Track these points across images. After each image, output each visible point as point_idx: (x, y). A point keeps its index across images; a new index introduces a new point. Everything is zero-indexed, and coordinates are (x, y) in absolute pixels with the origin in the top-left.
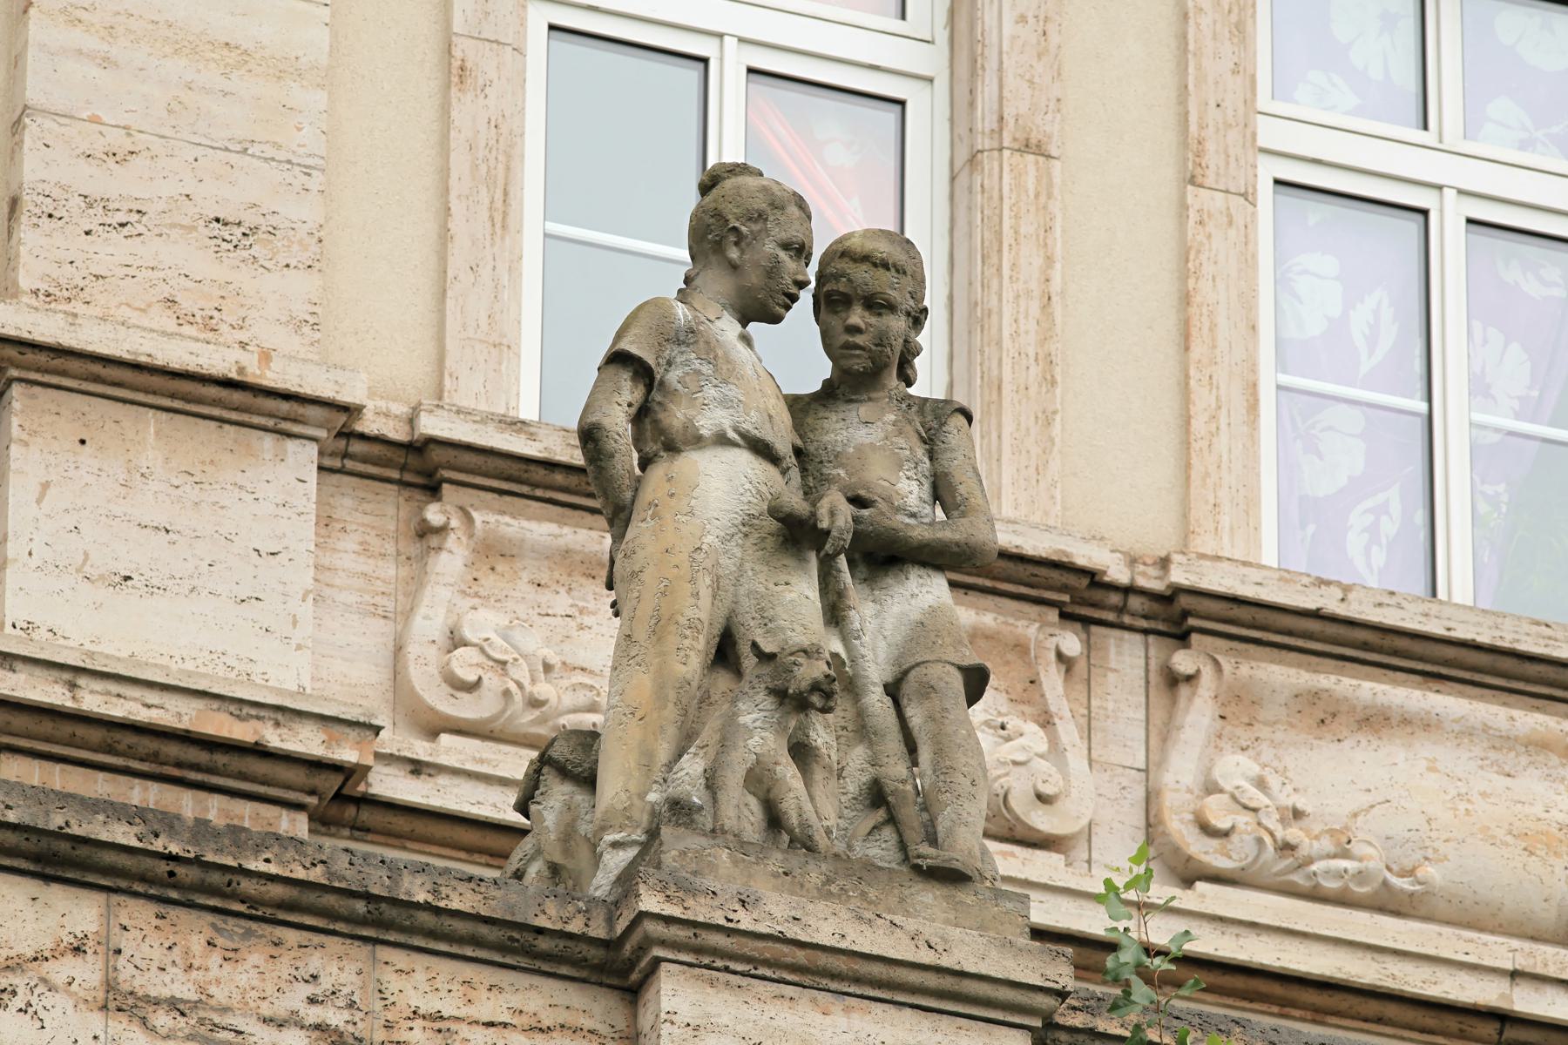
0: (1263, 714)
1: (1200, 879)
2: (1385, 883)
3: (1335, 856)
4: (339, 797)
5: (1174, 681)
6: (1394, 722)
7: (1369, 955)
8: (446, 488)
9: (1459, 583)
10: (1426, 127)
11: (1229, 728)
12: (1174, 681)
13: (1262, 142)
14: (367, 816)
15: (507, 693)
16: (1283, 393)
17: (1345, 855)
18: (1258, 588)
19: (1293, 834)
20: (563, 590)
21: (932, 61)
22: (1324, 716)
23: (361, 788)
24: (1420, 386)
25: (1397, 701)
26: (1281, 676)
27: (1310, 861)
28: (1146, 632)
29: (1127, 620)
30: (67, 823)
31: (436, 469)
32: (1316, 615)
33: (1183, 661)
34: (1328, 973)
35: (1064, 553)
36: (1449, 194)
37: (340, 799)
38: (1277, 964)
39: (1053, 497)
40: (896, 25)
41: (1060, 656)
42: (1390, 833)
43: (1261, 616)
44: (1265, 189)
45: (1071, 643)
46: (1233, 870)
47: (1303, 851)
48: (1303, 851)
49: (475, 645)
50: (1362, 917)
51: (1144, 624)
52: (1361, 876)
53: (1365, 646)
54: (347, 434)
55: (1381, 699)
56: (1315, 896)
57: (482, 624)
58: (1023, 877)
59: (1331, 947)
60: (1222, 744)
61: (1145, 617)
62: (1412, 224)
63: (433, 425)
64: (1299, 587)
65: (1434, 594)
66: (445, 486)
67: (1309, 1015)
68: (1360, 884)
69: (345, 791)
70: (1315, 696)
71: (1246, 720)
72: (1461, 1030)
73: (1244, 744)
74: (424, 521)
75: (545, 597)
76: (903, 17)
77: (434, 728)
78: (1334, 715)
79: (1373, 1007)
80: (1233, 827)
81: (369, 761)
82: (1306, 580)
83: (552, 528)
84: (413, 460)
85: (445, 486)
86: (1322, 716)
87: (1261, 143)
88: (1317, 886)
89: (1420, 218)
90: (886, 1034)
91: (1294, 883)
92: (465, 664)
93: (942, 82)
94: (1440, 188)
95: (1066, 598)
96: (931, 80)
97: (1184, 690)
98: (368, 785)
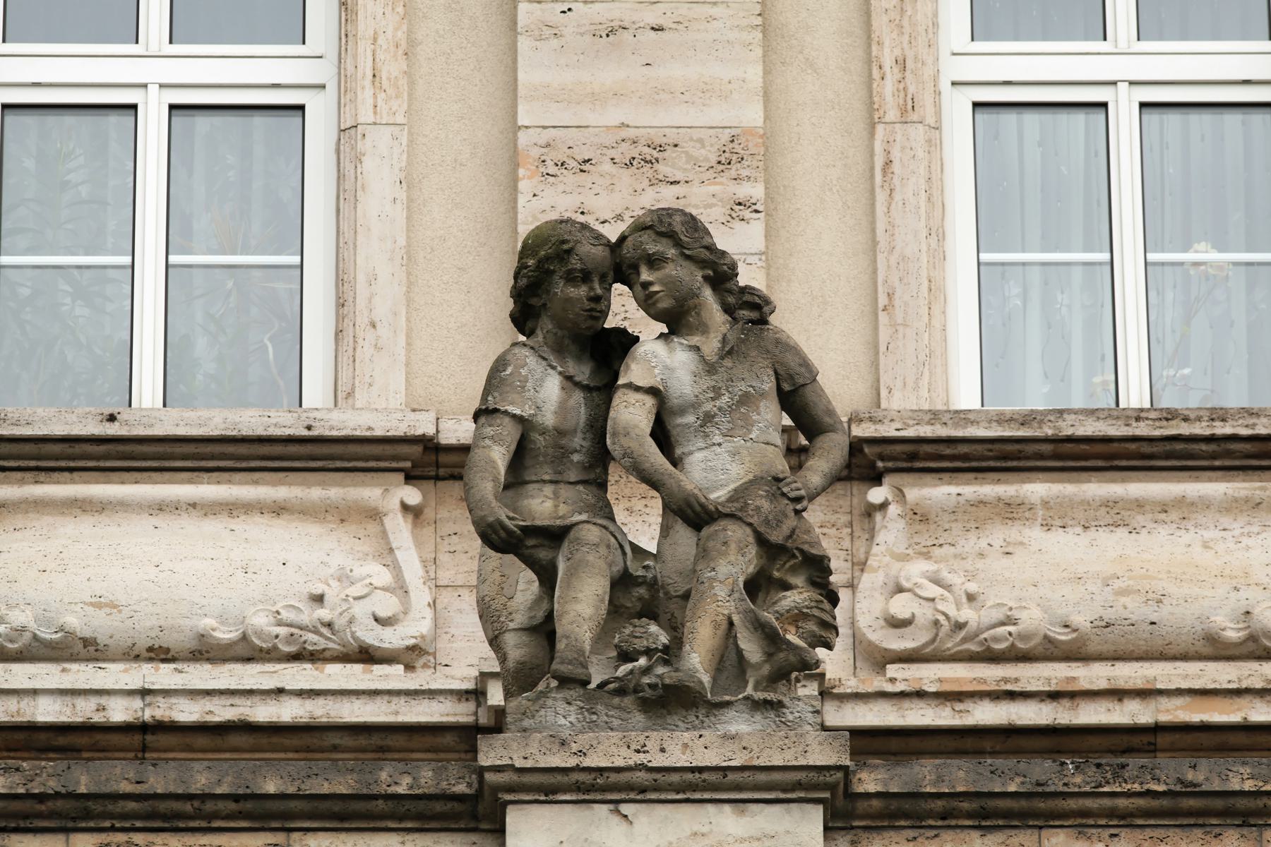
1: (893, 662)
5: (871, 511)
10: (1105, 39)
12: (871, 511)
15: (936, 623)
19: (324, 613)
21: (322, 72)
30: (1207, 779)
33: (877, 495)
36: (1123, 87)
38: (881, 724)
41: (405, 507)
44: (958, 108)
45: (412, 495)
46: (914, 650)
49: (909, 590)
53: (965, 457)
57: (915, 571)
58: (1173, 687)
65: (301, 406)
74: (424, 496)
77: (882, 660)
80: (913, 614)
83: (953, 489)
88: (989, 649)
90: (235, 843)
92: (901, 607)
94: (1114, 83)
97: (878, 517)
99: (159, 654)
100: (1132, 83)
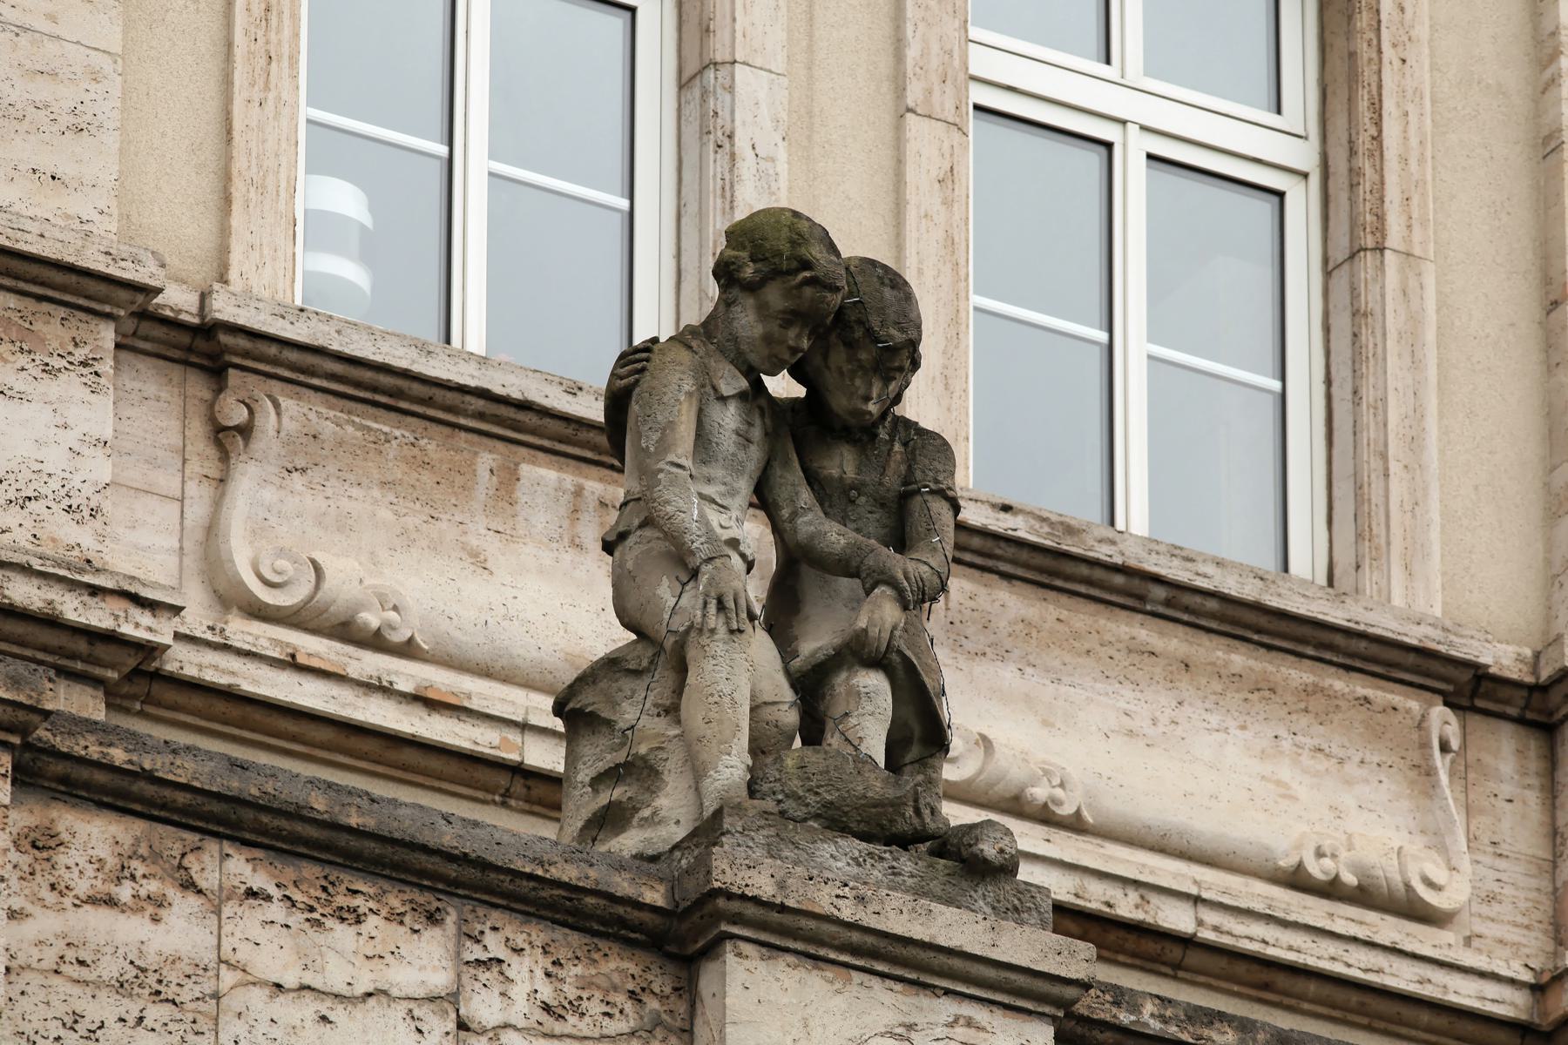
4: (137, 672)
8: (234, 376)
9: (473, 332)
10: (1108, 62)
13: (974, 70)
14: (157, 689)
21: (1304, 156)
23: (155, 664)
24: (446, 138)
31: (222, 352)
37: (138, 676)
40: (1271, 119)
54: (144, 315)
62: (1095, 157)
63: (224, 308)
65: (1286, 570)
66: (231, 371)
69: (143, 667)
72: (1363, 1004)
75: (1207, 716)
76: (1279, 112)
81: (167, 639)
84: (200, 344)
85: (231, 371)
87: (973, 71)
89: (628, 15)
93: (1315, 180)
94: (1124, 122)
95: (1450, 688)
96: (1305, 176)
98: (163, 662)
99: (1297, 880)
100: (1143, 128)
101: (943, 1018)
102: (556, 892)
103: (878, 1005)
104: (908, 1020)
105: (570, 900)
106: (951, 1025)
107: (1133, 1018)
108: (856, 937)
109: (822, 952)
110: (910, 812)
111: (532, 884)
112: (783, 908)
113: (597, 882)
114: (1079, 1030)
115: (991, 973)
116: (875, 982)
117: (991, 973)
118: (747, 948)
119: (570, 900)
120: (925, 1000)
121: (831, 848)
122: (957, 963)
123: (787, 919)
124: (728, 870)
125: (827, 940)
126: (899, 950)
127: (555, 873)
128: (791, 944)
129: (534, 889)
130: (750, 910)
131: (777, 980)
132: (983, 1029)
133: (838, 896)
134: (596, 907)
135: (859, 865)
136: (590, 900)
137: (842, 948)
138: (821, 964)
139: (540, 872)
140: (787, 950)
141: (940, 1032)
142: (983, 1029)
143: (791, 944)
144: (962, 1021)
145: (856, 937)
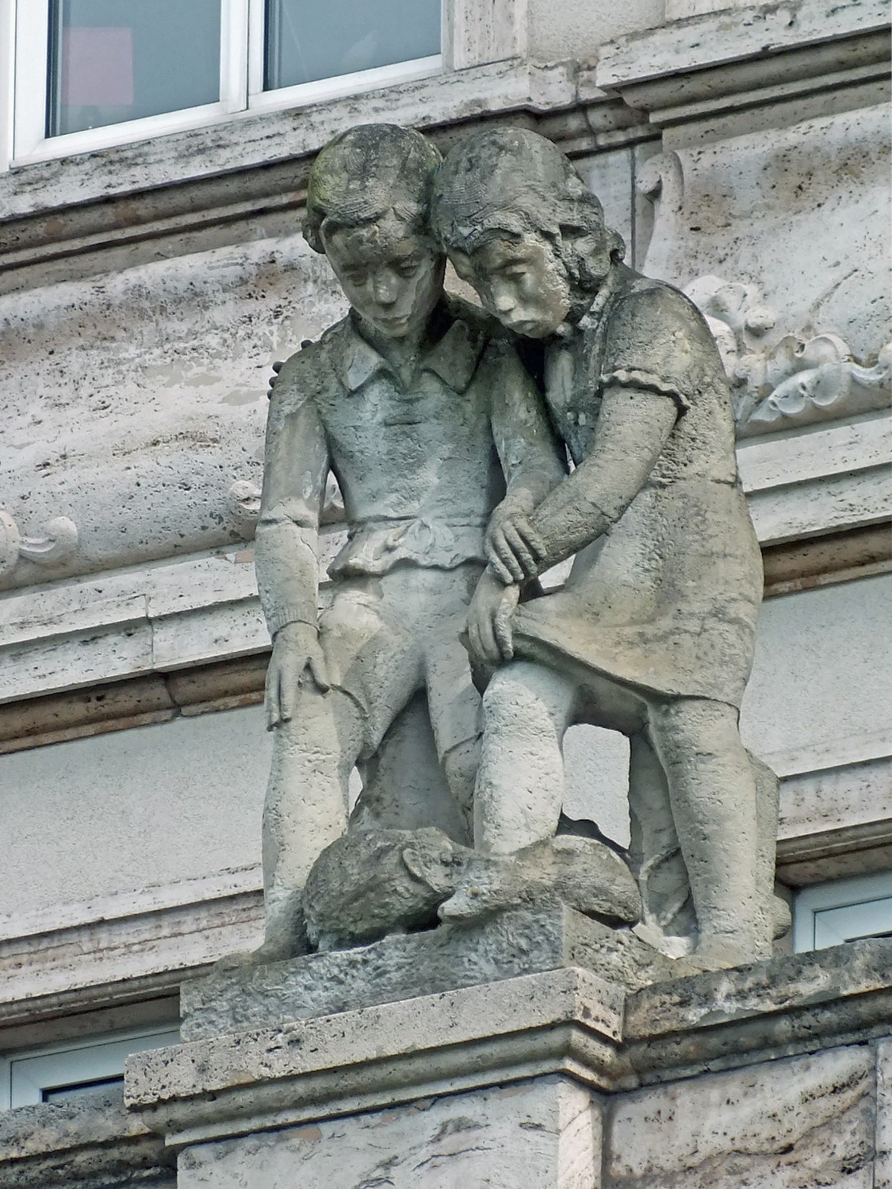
0: (740, 205)
2: (854, 381)
3: (794, 372)
6: (873, 156)
7: (824, 489)
11: (704, 240)
16: (74, 99)
17: (801, 366)
18: (695, 52)
20: (260, 262)
22: (800, 182)
25: (870, 127)
26: (746, 150)
27: (768, 388)
28: (630, 144)
29: (602, 141)
32: (765, 55)
34: (776, 535)
35: (478, 103)
39: (510, 16)
42: (852, 314)
43: (717, 80)
47: (756, 381)
48: (756, 381)
50: (840, 434)
51: (620, 137)
52: (820, 387)
53: (842, 66)
55: (855, 133)
56: (789, 427)
59: (781, 498)
60: (697, 265)
61: (621, 128)
64: (742, 29)
67: (799, 583)
68: (825, 394)
70: (782, 160)
71: (721, 221)
73: (721, 253)
78: (810, 175)
79: (854, 548)
82: (749, 16)
86: (797, 181)
88: (785, 416)
91: (759, 423)
101: (431, 1132)
102: (43, 1166)
103: (351, 1149)
104: (385, 1157)
105: (61, 1167)
106: (437, 1139)
107: (704, 1011)
108: (301, 1088)
109: (280, 1120)
110: (402, 884)
111: (17, 1168)
112: (213, 1095)
113: (77, 1135)
114: (653, 1053)
115: (461, 1058)
116: (349, 1126)
117: (461, 1058)
118: (201, 1153)
119: (61, 1167)
120: (406, 1122)
121: (305, 979)
122: (420, 1065)
123: (222, 1103)
124: (142, 1078)
125: (275, 1105)
126: (351, 1080)
127: (31, 1147)
128: (244, 1126)
129: (22, 1172)
130: (180, 1112)
131: (235, 1176)
132: (477, 1126)
133: (270, 1050)
134: (90, 1162)
135: (341, 982)
136: (81, 1158)
137: (300, 1103)
138: (284, 1133)
139: (14, 1154)
140: (243, 1135)
141: (423, 1154)
142: (477, 1126)
143: (244, 1126)
144: (450, 1128)
145: (301, 1088)
